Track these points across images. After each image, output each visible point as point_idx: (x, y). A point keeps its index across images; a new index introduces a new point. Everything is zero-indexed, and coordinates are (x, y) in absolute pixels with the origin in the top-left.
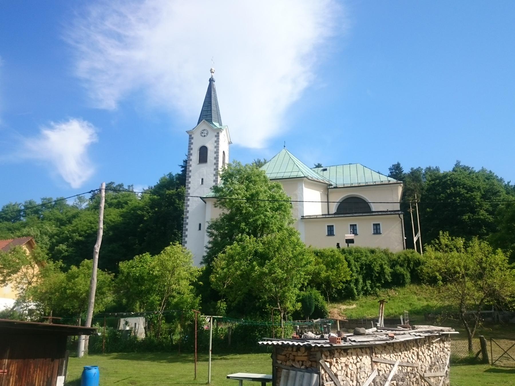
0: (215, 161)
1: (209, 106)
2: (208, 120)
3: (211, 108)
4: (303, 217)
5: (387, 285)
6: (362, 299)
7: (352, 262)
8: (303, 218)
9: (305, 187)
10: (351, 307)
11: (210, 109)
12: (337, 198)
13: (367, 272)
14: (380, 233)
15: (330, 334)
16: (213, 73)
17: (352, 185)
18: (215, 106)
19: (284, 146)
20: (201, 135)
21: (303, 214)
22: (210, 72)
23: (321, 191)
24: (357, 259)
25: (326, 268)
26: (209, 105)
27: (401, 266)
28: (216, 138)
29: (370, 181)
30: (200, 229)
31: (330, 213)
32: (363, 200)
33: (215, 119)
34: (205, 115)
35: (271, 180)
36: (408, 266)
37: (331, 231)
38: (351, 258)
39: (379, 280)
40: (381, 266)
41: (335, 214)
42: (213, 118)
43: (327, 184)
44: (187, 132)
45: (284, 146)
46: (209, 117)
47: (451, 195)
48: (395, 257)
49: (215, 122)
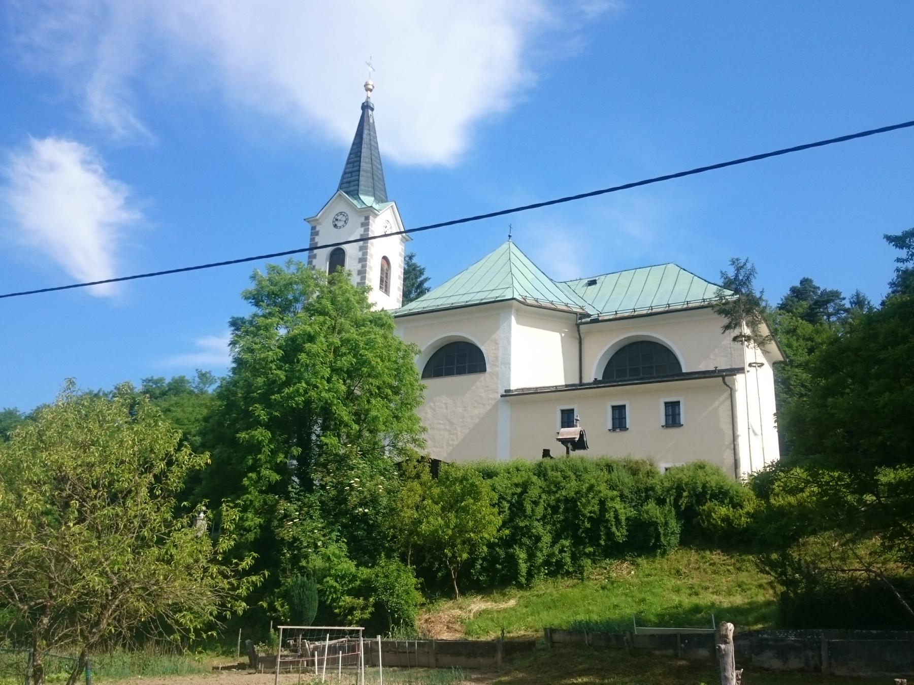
1: (356, 162)
2: (352, 191)
3: (360, 166)
4: (509, 391)
5: (615, 551)
8: (508, 394)
9: (518, 323)
10: (503, 606)
11: (356, 168)
13: (566, 520)
14: (680, 425)
16: (371, 90)
17: (633, 314)
18: (368, 160)
19: (510, 236)
21: (510, 385)
22: (364, 88)
23: (564, 332)
25: (889, 484)
26: (355, 159)
27: (661, 502)
28: (362, 229)
29: (677, 300)
31: (585, 381)
32: (666, 348)
33: (367, 188)
34: (347, 182)
35: (396, 317)
39: (593, 538)
42: (361, 188)
43: (576, 313)
44: (307, 220)
45: (510, 236)
46: (354, 186)
49: (367, 194)
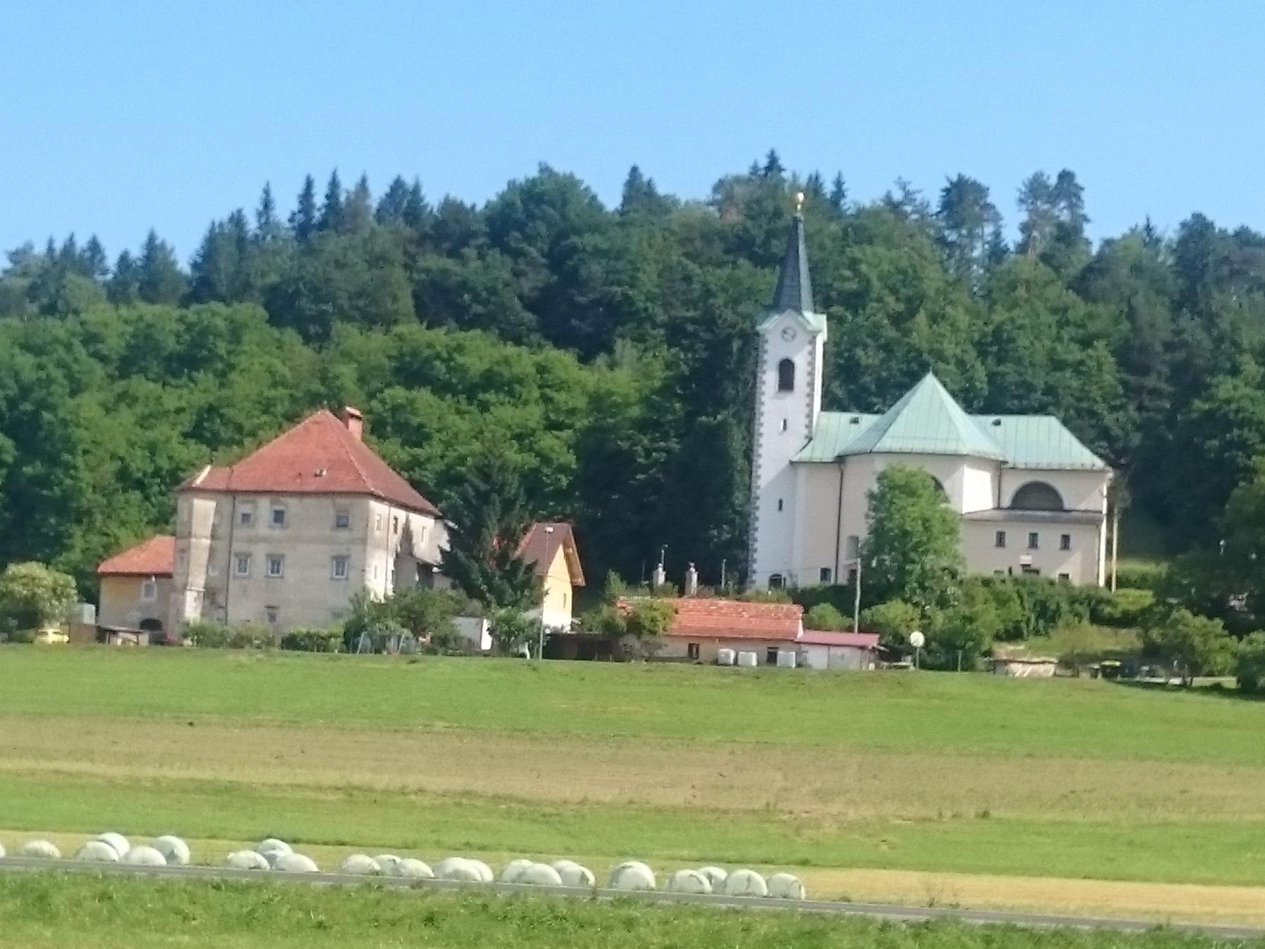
0: (808, 390)
6: (1033, 640)
7: (1025, 597)
12: (1012, 485)
15: (1164, 606)
20: (787, 341)
24: (1031, 594)
27: (1081, 604)
30: (780, 508)
36: (1089, 604)
37: (1000, 540)
38: (1024, 591)
40: (1058, 605)
41: (1009, 508)
47: (1230, 445)
48: (1076, 592)
